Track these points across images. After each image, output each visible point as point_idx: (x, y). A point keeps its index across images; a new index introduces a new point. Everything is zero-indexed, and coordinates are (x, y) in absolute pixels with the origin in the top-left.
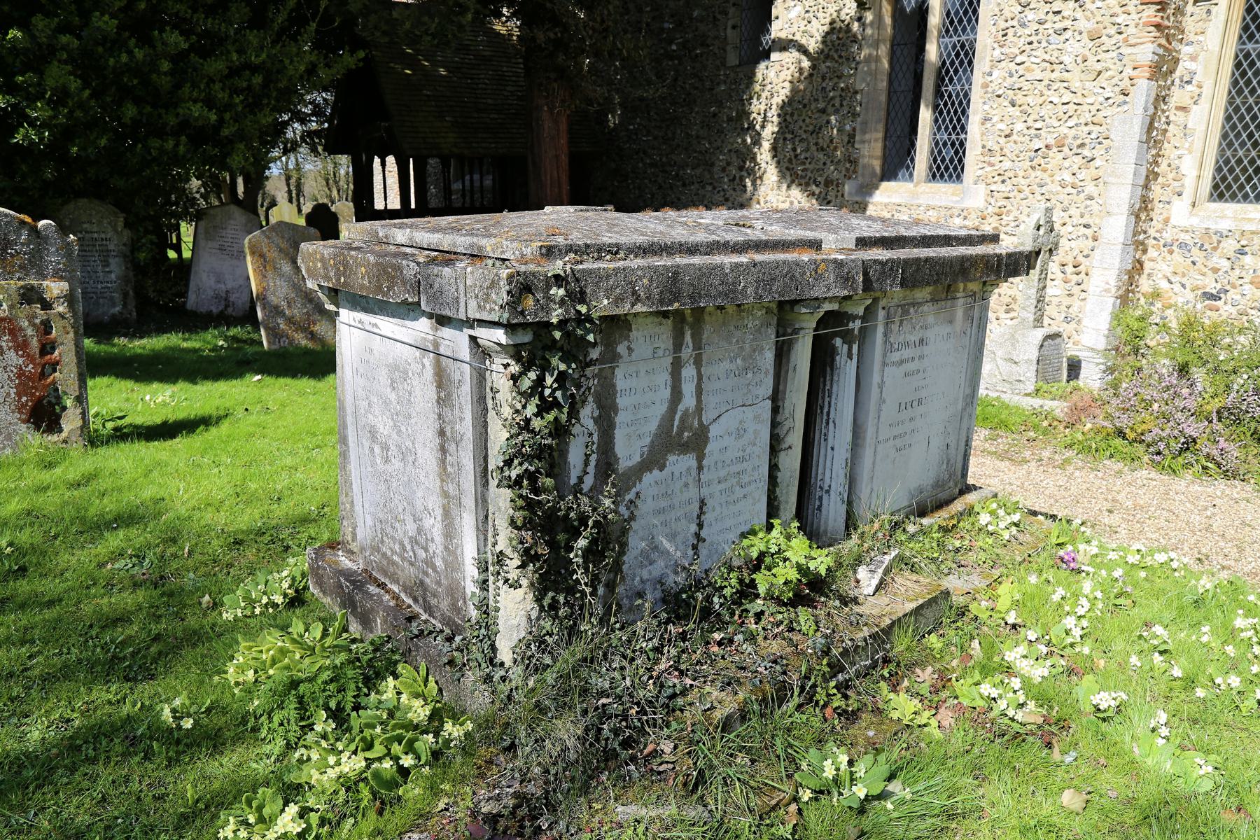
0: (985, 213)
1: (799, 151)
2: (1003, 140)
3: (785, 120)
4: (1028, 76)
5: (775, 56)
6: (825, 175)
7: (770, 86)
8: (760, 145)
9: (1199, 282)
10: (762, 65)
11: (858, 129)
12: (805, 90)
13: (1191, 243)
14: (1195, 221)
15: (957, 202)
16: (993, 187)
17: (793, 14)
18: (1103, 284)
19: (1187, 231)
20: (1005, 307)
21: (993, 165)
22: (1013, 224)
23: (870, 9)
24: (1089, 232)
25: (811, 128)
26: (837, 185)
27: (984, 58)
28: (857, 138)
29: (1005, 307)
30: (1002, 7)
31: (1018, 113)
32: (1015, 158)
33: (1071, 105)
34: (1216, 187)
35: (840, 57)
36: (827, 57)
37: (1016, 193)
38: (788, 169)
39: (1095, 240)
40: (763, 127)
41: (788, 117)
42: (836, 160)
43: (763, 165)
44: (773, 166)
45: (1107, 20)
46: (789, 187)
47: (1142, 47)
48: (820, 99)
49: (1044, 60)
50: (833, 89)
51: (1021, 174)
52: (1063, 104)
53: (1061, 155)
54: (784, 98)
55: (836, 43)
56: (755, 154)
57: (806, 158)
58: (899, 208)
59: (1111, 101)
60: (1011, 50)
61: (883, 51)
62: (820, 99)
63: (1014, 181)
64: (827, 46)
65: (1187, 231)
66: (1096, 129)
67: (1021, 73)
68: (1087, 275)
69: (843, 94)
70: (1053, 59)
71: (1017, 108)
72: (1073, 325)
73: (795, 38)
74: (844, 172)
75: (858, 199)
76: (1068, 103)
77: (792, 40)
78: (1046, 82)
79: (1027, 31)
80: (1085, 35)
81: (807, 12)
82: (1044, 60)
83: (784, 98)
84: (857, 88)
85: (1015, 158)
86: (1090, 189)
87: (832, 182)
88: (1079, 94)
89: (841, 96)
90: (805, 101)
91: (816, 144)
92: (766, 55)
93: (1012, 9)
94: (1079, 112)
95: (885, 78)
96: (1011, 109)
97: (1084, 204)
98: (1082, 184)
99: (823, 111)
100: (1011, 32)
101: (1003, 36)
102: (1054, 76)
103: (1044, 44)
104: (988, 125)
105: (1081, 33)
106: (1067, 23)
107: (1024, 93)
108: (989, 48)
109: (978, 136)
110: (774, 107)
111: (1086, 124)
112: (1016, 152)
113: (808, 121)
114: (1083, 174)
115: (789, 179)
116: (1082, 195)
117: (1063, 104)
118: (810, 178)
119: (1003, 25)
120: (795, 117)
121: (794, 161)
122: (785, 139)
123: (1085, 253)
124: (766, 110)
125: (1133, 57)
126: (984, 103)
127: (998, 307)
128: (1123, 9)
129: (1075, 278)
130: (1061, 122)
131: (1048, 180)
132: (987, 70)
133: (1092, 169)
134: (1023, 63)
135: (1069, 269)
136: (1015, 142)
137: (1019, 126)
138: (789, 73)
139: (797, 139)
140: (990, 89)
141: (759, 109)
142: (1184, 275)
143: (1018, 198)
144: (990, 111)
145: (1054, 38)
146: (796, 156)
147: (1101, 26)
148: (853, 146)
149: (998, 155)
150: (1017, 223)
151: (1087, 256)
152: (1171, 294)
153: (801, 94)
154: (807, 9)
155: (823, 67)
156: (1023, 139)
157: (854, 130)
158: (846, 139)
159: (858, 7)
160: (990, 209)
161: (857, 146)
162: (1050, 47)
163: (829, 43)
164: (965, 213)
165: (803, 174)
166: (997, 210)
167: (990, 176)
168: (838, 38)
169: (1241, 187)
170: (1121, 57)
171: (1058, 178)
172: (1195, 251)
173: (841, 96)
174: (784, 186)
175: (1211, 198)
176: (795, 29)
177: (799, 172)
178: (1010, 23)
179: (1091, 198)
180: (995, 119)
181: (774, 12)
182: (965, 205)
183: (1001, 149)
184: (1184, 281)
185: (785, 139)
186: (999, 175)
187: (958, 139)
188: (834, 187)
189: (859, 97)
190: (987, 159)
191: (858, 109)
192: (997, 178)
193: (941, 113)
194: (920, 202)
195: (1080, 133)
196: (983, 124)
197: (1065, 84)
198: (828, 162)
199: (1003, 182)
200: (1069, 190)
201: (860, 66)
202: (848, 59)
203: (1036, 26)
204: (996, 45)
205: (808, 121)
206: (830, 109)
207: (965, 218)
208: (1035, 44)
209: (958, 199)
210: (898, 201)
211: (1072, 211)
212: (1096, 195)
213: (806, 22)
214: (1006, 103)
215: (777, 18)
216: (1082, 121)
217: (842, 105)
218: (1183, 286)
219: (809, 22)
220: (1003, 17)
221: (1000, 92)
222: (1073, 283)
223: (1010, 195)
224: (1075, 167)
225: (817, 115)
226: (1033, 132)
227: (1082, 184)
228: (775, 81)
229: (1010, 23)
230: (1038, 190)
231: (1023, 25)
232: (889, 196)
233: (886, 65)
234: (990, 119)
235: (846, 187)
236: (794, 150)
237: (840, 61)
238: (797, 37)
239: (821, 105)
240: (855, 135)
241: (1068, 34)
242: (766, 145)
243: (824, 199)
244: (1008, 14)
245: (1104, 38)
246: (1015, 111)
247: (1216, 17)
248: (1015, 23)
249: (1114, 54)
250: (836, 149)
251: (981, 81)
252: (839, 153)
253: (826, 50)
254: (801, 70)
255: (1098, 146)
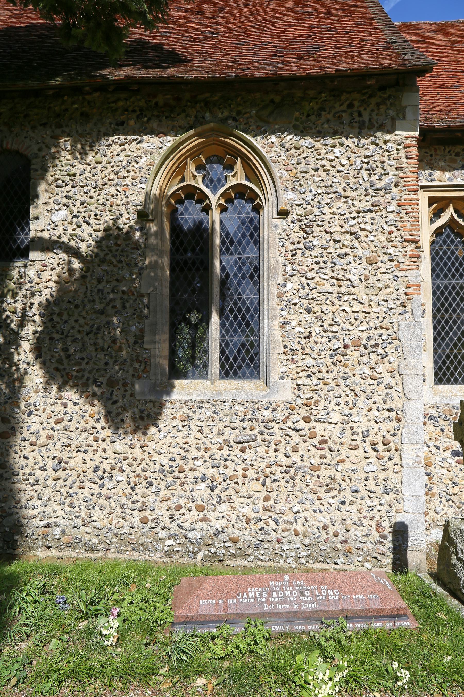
0: (294, 404)
1: (72, 351)
2: (303, 341)
3: (52, 320)
4: (320, 289)
5: (34, 255)
6: (108, 376)
7: (28, 285)
8: (19, 346)
9: (448, 444)
10: (19, 264)
11: (147, 329)
12: (76, 291)
13: (436, 415)
14: (437, 400)
15: (264, 396)
16: (299, 382)
17: (58, 217)
18: (414, 457)
19: (433, 407)
20: (325, 487)
21: (297, 363)
22: (323, 413)
23: (152, 221)
24: (393, 415)
25: (87, 328)
26: (125, 385)
27: (277, 272)
28: (146, 339)
29: (325, 487)
30: (288, 232)
31: (314, 319)
32: (316, 356)
33: (361, 313)
34: (436, 374)
35: (120, 261)
36: (103, 261)
37: (322, 386)
38: (57, 369)
39: (399, 420)
40: (21, 325)
41: (55, 317)
42: (120, 360)
43: (23, 366)
44: (37, 367)
45: (379, 250)
46: (60, 389)
47: (411, 272)
48: (97, 300)
49: (332, 277)
50: (113, 291)
51: (324, 369)
52: (353, 312)
53: (357, 354)
54: (49, 297)
55: (115, 248)
56: (12, 354)
57: (83, 359)
58: (201, 405)
59: (394, 311)
60: (300, 267)
61: (166, 261)
62: (97, 300)
63: (320, 375)
64: (102, 250)
65: (433, 407)
66: (385, 332)
67: (312, 286)
68: (397, 450)
69: (125, 297)
70: (340, 277)
71: (311, 314)
72: (392, 495)
73: (61, 240)
74: (131, 372)
75: (153, 398)
76: (358, 312)
77: (57, 242)
78: (336, 295)
79: (314, 253)
80: (364, 260)
81: (76, 217)
82: (332, 277)
83: (49, 297)
84: (143, 291)
85: (316, 356)
86: (388, 379)
87: (117, 382)
88: (366, 305)
89: (122, 298)
90: (78, 302)
91: (95, 344)
92: (24, 254)
93: (298, 235)
94: (368, 319)
95: (168, 284)
96: (307, 315)
97: (385, 392)
98: (380, 376)
99: (102, 312)
100: (299, 253)
101: (293, 255)
102: (342, 290)
103: (329, 265)
104: (287, 328)
105: (360, 259)
106: (348, 250)
107: (318, 302)
108: (281, 264)
109: (279, 338)
110: (36, 306)
111: (376, 329)
112: (318, 351)
113: (81, 321)
114: (380, 368)
115: (60, 381)
116: (382, 385)
117: (353, 312)
118: (88, 379)
119: (291, 247)
120: (65, 317)
121: (65, 361)
122: (51, 339)
123: (392, 432)
124: (24, 309)
125: (406, 279)
126: (282, 310)
127: (318, 488)
128: (391, 243)
129: (387, 455)
130: (354, 327)
131: (351, 374)
132: (281, 282)
133: (387, 364)
134: (313, 278)
135: (380, 447)
136: (315, 343)
137: (318, 330)
138: (54, 273)
139: (69, 339)
140: (285, 298)
141: (16, 308)
142: (436, 439)
143: (325, 390)
144: (288, 316)
145: (337, 260)
146: (68, 357)
147: (375, 254)
148: (141, 347)
149: (300, 353)
150: (326, 412)
151: (395, 435)
152: (431, 455)
153: (72, 294)
154: (76, 213)
155: (99, 271)
156: (322, 340)
157: (142, 331)
158: (132, 340)
159: (138, 218)
160: (299, 401)
161: (146, 346)
162: (337, 267)
163: (104, 248)
164: (274, 406)
165: (79, 375)
166: (305, 402)
167: (294, 372)
168: (116, 244)
169: (452, 374)
170: (396, 278)
171: (358, 372)
172: (441, 421)
173: (122, 298)
174: (54, 389)
175: (222, 378)
176: (60, 231)
177: (74, 374)
178: (297, 246)
179: (390, 388)
180: (294, 323)
181: (33, 212)
182: (272, 399)
183: (303, 349)
184: (437, 444)
185: (51, 339)
186: (304, 370)
187: (248, 341)
188: (120, 386)
189: (146, 300)
190: (290, 357)
191: (146, 311)
192: (301, 374)
193: (227, 318)
194: (224, 398)
195: (371, 335)
196: (282, 327)
197: (355, 297)
198: (111, 362)
199: (309, 377)
200: (369, 381)
201: (145, 272)
202: (128, 265)
203: (321, 251)
204: (287, 262)
205: (81, 321)
206: (109, 310)
207: (274, 410)
208: (322, 265)
209: (264, 393)
210: (199, 398)
211: (376, 398)
212: (393, 384)
213: (74, 226)
214: (302, 310)
215: (37, 218)
216: (372, 325)
217: (124, 307)
218: (438, 448)
219: (79, 227)
220: (291, 241)
221: (296, 300)
222: (386, 459)
223: (317, 388)
224: (373, 363)
225: (94, 316)
226: (329, 334)
227: (380, 376)
228: (35, 279)
229: (297, 246)
230: (342, 382)
231: (310, 249)
232: (188, 394)
233: (168, 273)
234: (289, 323)
235: (137, 387)
236: (65, 350)
237: (120, 265)
238: (64, 239)
239: (98, 307)
240: (143, 337)
241: (350, 258)
242: (26, 345)
243: (108, 399)
244: (294, 237)
245: (380, 264)
246: (311, 317)
247: (424, 260)
248: (301, 246)
249: (391, 276)
250: (120, 349)
251: (276, 291)
252: (124, 353)
253: (102, 255)
254: (71, 271)
255: (389, 346)
